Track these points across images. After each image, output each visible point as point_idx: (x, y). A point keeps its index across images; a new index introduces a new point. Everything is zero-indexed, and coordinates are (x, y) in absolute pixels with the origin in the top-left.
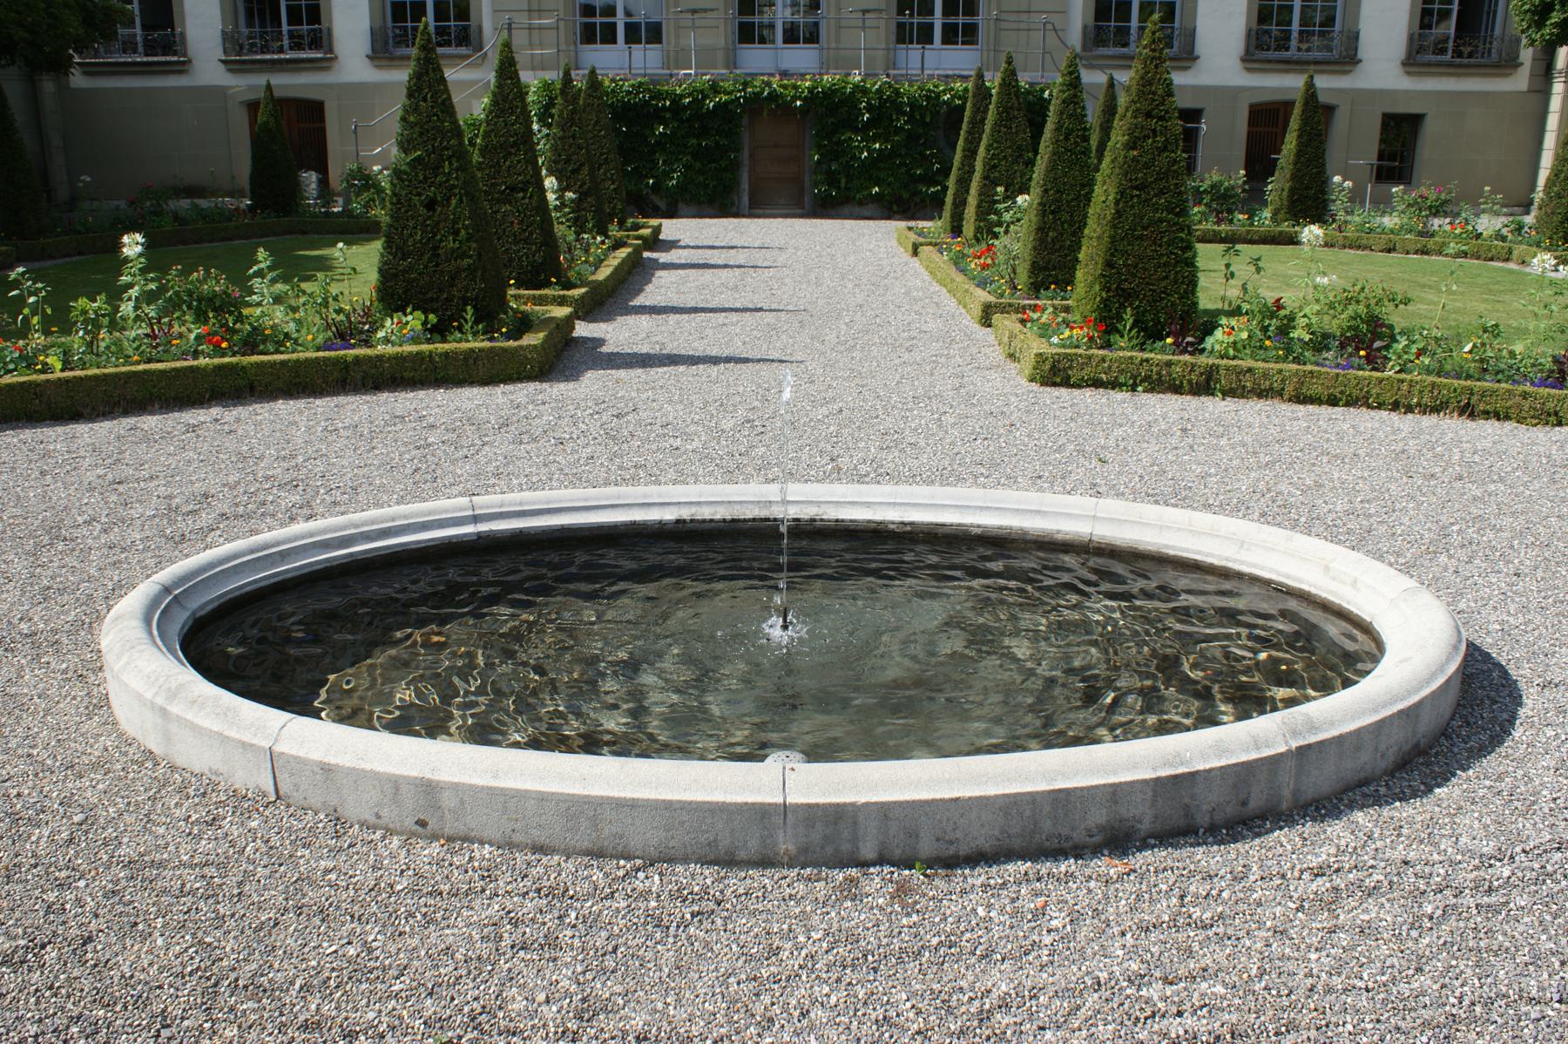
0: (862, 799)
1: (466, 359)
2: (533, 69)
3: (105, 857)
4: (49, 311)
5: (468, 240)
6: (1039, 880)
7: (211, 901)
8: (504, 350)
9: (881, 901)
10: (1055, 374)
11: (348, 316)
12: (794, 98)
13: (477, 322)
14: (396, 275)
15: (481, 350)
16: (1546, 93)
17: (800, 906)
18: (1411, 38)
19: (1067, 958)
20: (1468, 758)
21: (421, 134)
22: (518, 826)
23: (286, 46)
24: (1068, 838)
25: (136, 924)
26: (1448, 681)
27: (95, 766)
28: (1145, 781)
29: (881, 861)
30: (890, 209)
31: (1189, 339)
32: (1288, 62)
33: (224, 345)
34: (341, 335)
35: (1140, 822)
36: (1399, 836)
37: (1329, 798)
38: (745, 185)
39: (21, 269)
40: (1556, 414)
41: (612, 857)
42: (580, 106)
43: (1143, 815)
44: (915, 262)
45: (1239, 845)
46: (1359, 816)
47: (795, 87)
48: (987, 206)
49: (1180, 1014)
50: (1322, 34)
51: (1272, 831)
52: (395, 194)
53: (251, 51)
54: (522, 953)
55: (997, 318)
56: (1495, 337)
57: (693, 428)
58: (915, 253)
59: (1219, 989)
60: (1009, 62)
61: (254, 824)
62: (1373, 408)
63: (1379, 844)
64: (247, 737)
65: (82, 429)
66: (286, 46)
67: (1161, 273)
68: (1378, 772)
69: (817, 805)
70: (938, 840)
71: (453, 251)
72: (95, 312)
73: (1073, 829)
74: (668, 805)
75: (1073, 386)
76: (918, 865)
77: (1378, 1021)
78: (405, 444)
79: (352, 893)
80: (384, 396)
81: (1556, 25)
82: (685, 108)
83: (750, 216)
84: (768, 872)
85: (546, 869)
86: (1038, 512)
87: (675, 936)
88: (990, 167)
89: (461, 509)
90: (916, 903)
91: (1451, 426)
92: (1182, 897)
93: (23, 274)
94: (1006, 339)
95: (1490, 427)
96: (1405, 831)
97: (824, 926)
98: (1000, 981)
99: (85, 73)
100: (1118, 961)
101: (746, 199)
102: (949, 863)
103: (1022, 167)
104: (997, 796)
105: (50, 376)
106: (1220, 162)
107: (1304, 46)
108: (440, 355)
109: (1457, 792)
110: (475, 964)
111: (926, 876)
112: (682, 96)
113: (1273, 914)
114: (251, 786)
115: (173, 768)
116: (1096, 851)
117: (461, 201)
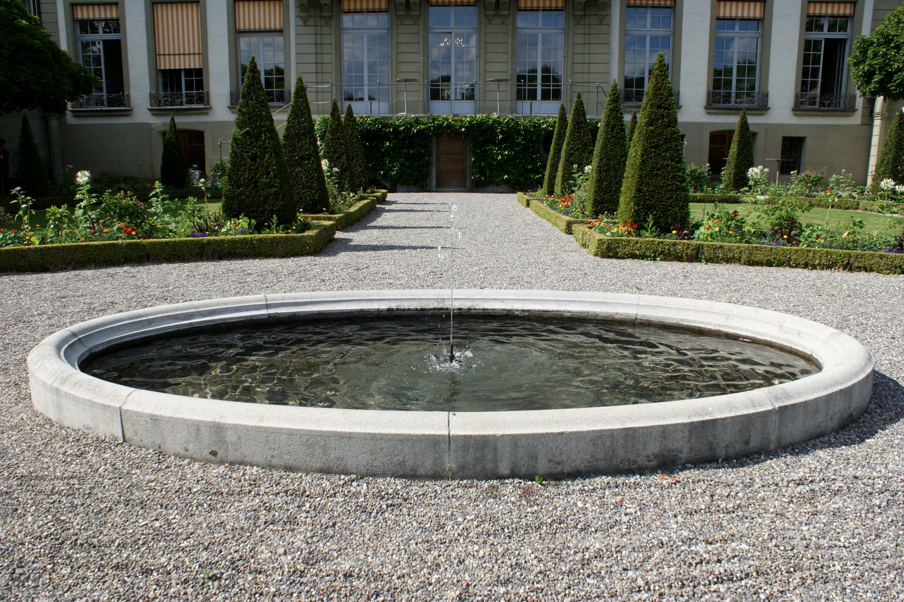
0: (500, 432)
1: (272, 243)
2: (318, 114)
3: (6, 474)
5: (275, 178)
6: (617, 487)
7: (70, 497)
8: (294, 238)
9: (513, 499)
10: (609, 251)
11: (205, 221)
12: (461, 127)
13: (278, 225)
14: (233, 197)
15: (280, 238)
16: (871, 125)
17: (461, 504)
18: (796, 96)
19: (639, 530)
20: (884, 424)
21: (249, 119)
22: (275, 453)
23: (184, 102)
24: (635, 462)
25: (17, 510)
26: (868, 376)
27: (12, 428)
28: (683, 424)
29: (513, 475)
30: (514, 188)
31: (686, 232)
32: (730, 109)
33: (133, 233)
34: (201, 230)
35: (681, 452)
36: (848, 463)
38: (434, 175)
39: (18, 188)
40: (900, 267)
41: (336, 473)
42: (343, 128)
43: (682, 447)
44: (529, 209)
45: (745, 468)
46: (820, 453)
47: (461, 121)
49: (719, 561)
50: (748, 95)
52: (233, 152)
54: (271, 526)
55: (575, 227)
56: (862, 227)
57: (400, 275)
58: (528, 205)
59: (744, 546)
60: (579, 97)
61: (107, 456)
62: (793, 267)
63: (836, 468)
64: (106, 402)
65: (48, 277)
66: (184, 102)
69: (471, 436)
70: (550, 461)
71: (266, 184)
72: (61, 214)
74: (373, 437)
75: (619, 258)
76: (537, 478)
77: (857, 565)
78: (233, 281)
79: (164, 493)
80: (224, 262)
81: (877, 82)
82: (401, 132)
84: (438, 483)
85: (291, 481)
86: (604, 303)
87: (375, 517)
88: (569, 155)
90: (536, 500)
91: (839, 276)
92: (712, 496)
93: (19, 191)
94: (580, 236)
95: (862, 276)
96: (852, 461)
97: (475, 512)
98: (595, 543)
99: (75, 116)
100: (674, 530)
101: (434, 183)
102: (558, 477)
103: (587, 154)
104: (588, 432)
105: (31, 246)
106: (696, 161)
107: (739, 101)
108: (257, 240)
109: (880, 441)
110: (239, 533)
111: (542, 485)
112: (399, 126)
113: (774, 505)
114: (108, 434)
115: (61, 428)
116: (653, 471)
117: (271, 155)
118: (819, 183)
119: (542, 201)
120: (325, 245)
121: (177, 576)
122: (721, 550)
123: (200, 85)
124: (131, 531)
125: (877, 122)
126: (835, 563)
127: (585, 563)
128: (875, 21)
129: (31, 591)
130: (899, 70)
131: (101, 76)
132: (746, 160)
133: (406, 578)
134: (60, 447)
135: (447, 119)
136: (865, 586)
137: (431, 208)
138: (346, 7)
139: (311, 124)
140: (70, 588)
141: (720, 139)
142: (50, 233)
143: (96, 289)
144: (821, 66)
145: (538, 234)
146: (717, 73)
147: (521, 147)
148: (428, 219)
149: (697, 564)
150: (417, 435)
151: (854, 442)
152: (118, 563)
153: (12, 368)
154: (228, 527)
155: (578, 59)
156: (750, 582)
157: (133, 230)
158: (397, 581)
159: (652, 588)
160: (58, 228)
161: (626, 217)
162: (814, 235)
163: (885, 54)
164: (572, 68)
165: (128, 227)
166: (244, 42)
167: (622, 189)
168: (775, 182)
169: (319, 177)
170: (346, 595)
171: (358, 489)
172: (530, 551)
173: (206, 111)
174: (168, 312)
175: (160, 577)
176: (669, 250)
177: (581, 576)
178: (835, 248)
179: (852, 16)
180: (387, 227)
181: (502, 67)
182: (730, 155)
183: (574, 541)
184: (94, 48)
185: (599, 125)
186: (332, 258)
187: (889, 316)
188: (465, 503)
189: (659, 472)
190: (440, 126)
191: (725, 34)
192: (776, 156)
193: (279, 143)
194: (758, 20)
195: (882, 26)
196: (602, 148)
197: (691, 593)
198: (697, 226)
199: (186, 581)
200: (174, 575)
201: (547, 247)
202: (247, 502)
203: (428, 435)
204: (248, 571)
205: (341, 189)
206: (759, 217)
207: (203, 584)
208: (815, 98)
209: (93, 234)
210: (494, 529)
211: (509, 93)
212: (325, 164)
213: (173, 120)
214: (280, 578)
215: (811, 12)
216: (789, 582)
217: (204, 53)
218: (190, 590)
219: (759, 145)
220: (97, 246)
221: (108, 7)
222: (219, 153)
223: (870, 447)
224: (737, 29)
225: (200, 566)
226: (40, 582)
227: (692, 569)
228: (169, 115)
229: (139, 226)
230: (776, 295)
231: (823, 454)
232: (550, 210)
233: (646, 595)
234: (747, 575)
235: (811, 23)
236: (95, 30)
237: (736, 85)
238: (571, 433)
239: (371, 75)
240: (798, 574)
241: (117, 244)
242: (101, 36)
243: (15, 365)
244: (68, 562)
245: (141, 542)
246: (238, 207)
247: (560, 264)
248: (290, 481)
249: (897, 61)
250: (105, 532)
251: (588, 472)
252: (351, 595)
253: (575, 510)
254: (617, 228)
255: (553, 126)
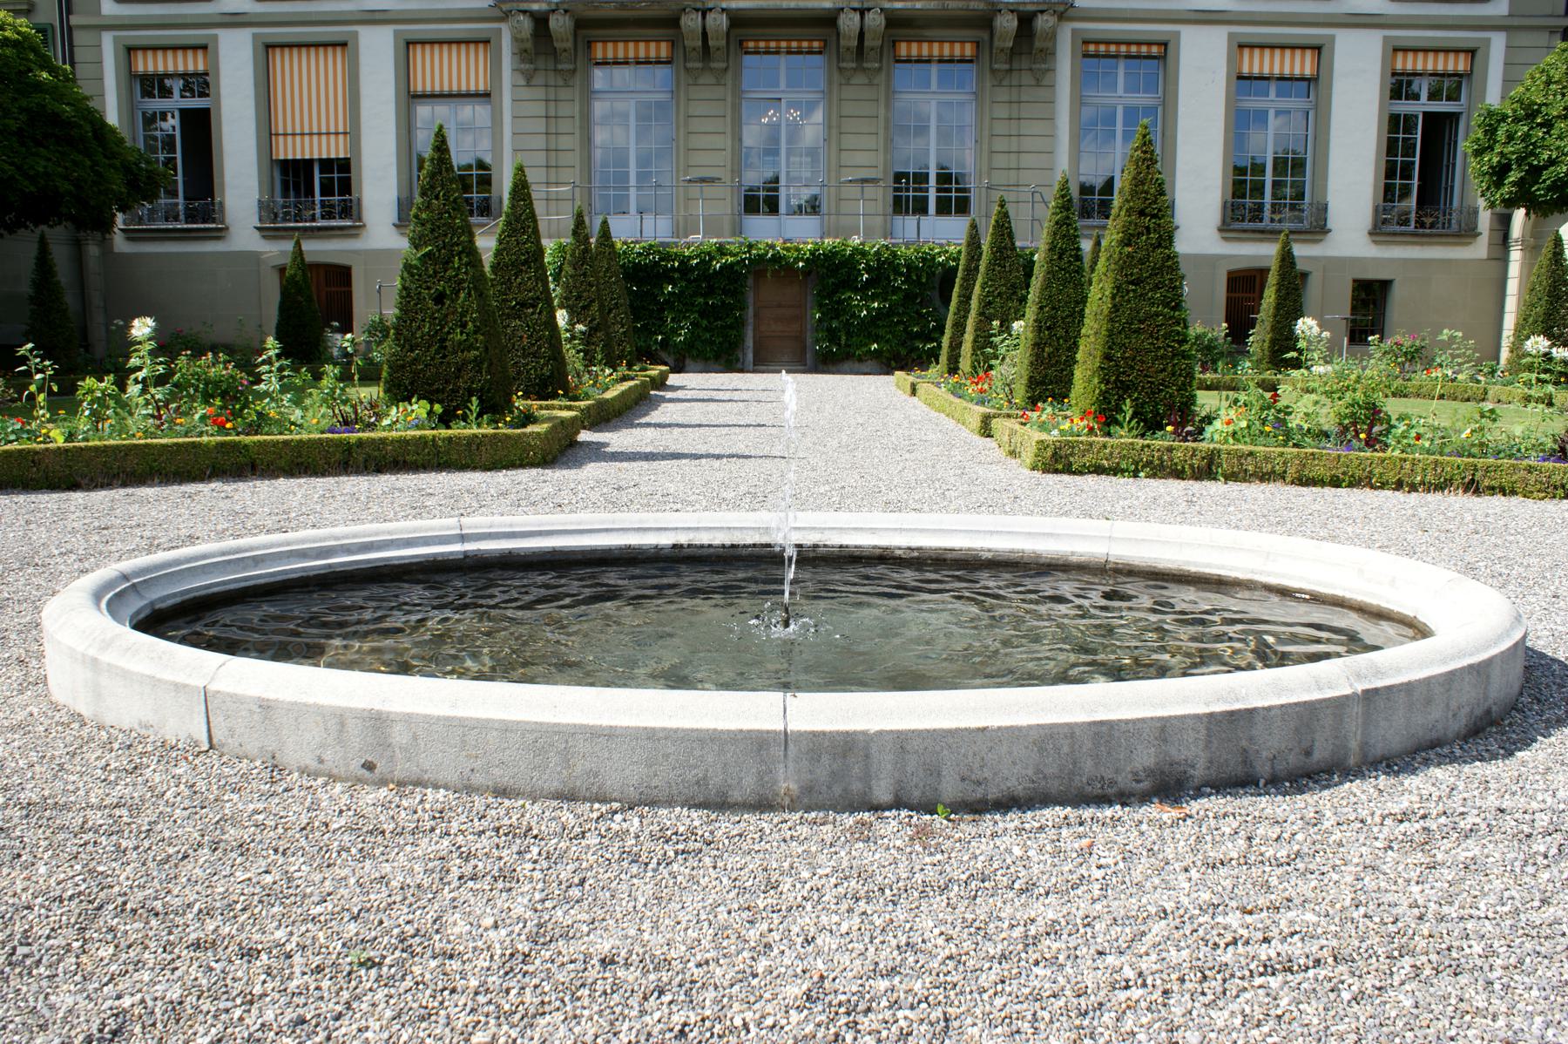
0: (874, 727)
1: (469, 444)
4: (55, 389)
5: (475, 332)
6: (1081, 824)
7: (114, 837)
8: (507, 436)
9: (898, 843)
10: (1057, 461)
12: (797, 260)
13: (480, 415)
14: (403, 367)
16: (1504, 260)
17: (808, 851)
18: (1376, 210)
20: (1547, 728)
21: (433, 231)
24: (1112, 783)
25: (19, 856)
28: (1197, 717)
29: (898, 804)
30: (889, 365)
31: (1189, 428)
32: (1262, 232)
34: (346, 422)
36: (1487, 789)
37: (1399, 756)
38: (749, 342)
39: (30, 345)
40: (1563, 486)
41: (585, 800)
42: (591, 253)
43: (1195, 756)
45: (1306, 796)
46: (1437, 772)
47: (798, 250)
48: (983, 341)
49: (1266, 940)
50: (1293, 207)
51: (1341, 783)
52: (404, 288)
53: (285, 220)
54: (470, 884)
55: (996, 424)
56: (1495, 420)
58: (914, 392)
59: (1310, 917)
62: (1376, 488)
64: (181, 678)
65: (78, 497)
67: (1158, 366)
68: (1450, 735)
69: (824, 733)
71: (460, 343)
72: (103, 392)
73: (1117, 771)
74: (651, 734)
75: (1074, 473)
76: (940, 808)
78: (401, 506)
79: (280, 830)
81: (1514, 184)
82: (693, 269)
83: (754, 371)
86: (1051, 535)
87: (655, 870)
88: (986, 304)
89: (448, 528)
91: (1457, 502)
92: (1249, 839)
93: (31, 351)
94: (1006, 438)
95: (1498, 501)
96: (1492, 785)
97: (833, 863)
98: (1047, 911)
99: (128, 239)
100: (1185, 892)
101: (750, 356)
102: (977, 808)
103: (1016, 303)
104: (1030, 727)
106: (1206, 320)
107: (1277, 217)
108: (444, 440)
109: (1541, 755)
110: (412, 894)
112: (690, 258)
113: (1358, 852)
114: (182, 737)
116: (1145, 798)
117: (469, 294)
118: (1416, 357)
119: (938, 385)
120: (562, 451)
121: (303, 961)
122: (1268, 922)
123: (346, 187)
124: (221, 890)
125: (1516, 255)
126: (1472, 942)
127: (1030, 942)
128: (1508, 82)
129: (44, 983)
130: (1552, 162)
131: (175, 170)
132: (1291, 307)
133: (712, 965)
134: (98, 758)
135: (772, 247)
136: (1526, 979)
137: (745, 396)
138: (599, 55)
139: (540, 251)
140: (112, 979)
141: (1244, 284)
142: (83, 424)
143: (162, 516)
144: (1417, 159)
145: (931, 436)
146: (1239, 170)
147: (901, 295)
148: (740, 414)
149: (1227, 945)
150: (729, 731)
151: (1494, 757)
152: (199, 939)
153: (14, 636)
154: (394, 883)
155: (1000, 144)
156: (1323, 973)
157: (228, 420)
158: (695, 971)
159: (1149, 982)
160: (97, 417)
161: (1085, 403)
162: (1413, 434)
163: (1526, 137)
164: (990, 159)
165: (219, 415)
166: (423, 111)
167: (1078, 356)
168: (1341, 355)
169: (551, 336)
170: (605, 993)
171: (625, 825)
172: (931, 924)
173: (355, 231)
174: (288, 544)
175: (274, 963)
176: (1160, 459)
177: (1023, 963)
178: (1450, 455)
179: (1468, 75)
180: (670, 425)
181: (867, 156)
182: (1260, 308)
183: (1008, 910)
184: (164, 125)
185: (1036, 257)
186: (573, 471)
187: (1548, 562)
188: (813, 849)
189: (1156, 800)
190: (761, 257)
191: (1253, 103)
192: (1342, 309)
193: (483, 274)
194: (1308, 80)
195: (1521, 89)
196: (1043, 290)
197: (1219, 989)
198: (1209, 420)
199: (319, 969)
200: (297, 959)
201: (949, 456)
202: (425, 845)
203: (749, 731)
204: (429, 953)
205: (589, 360)
206: (1317, 403)
207: (350, 973)
208: (1408, 213)
209: (158, 427)
210: (864, 889)
211: (880, 203)
212: (562, 317)
213: (298, 244)
214: (487, 964)
215: (1399, 66)
216: (1392, 974)
217: (353, 133)
218: (326, 984)
219: (1313, 292)
220: (163, 446)
221: (190, 53)
222: (377, 301)
223: (1523, 763)
224: (1272, 95)
225: (344, 945)
226: (61, 969)
227: (1219, 952)
228: (291, 237)
229: (237, 414)
230: (1350, 530)
231: (1442, 774)
232: (952, 398)
233: (1141, 992)
234: (1317, 962)
235: (1400, 86)
236: (166, 93)
237: (1270, 191)
238: (999, 728)
239: (639, 167)
240: (1407, 961)
241: (200, 444)
242: (177, 102)
243: (20, 632)
244: (109, 937)
245: (239, 906)
246: (411, 384)
247: (972, 482)
248: (503, 812)
249: (1547, 148)
250: (176, 892)
251: (1031, 799)
252: (613, 992)
253: (1009, 861)
254: (1069, 423)
255: (957, 259)
